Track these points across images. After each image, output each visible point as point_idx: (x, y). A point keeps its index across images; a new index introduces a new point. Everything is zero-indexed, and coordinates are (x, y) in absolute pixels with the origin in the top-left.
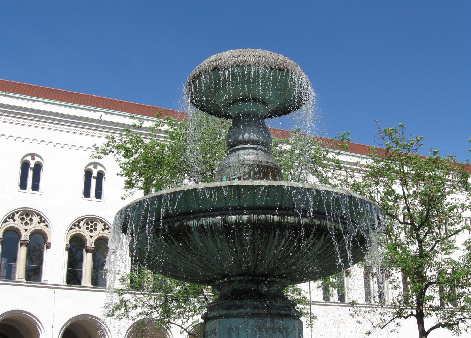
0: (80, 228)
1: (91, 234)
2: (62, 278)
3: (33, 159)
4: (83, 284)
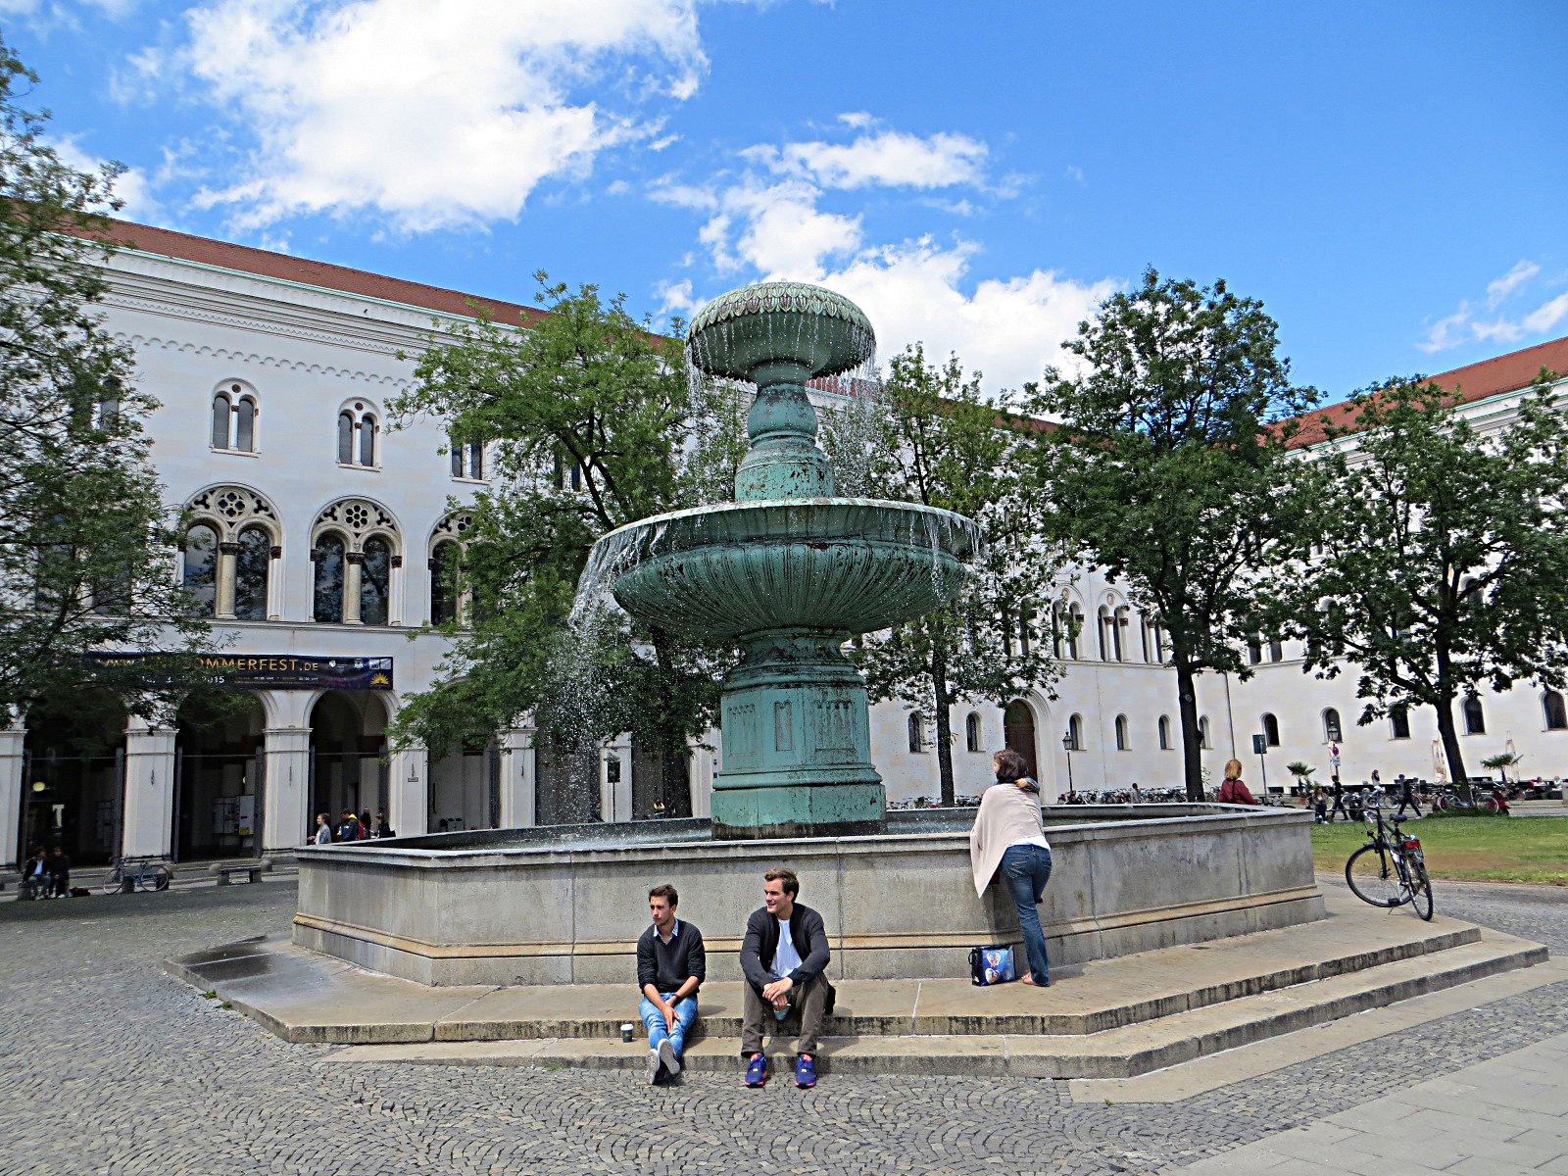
0: (335, 519)
1: (357, 531)
2: (306, 612)
3: (236, 389)
4: (273, 609)
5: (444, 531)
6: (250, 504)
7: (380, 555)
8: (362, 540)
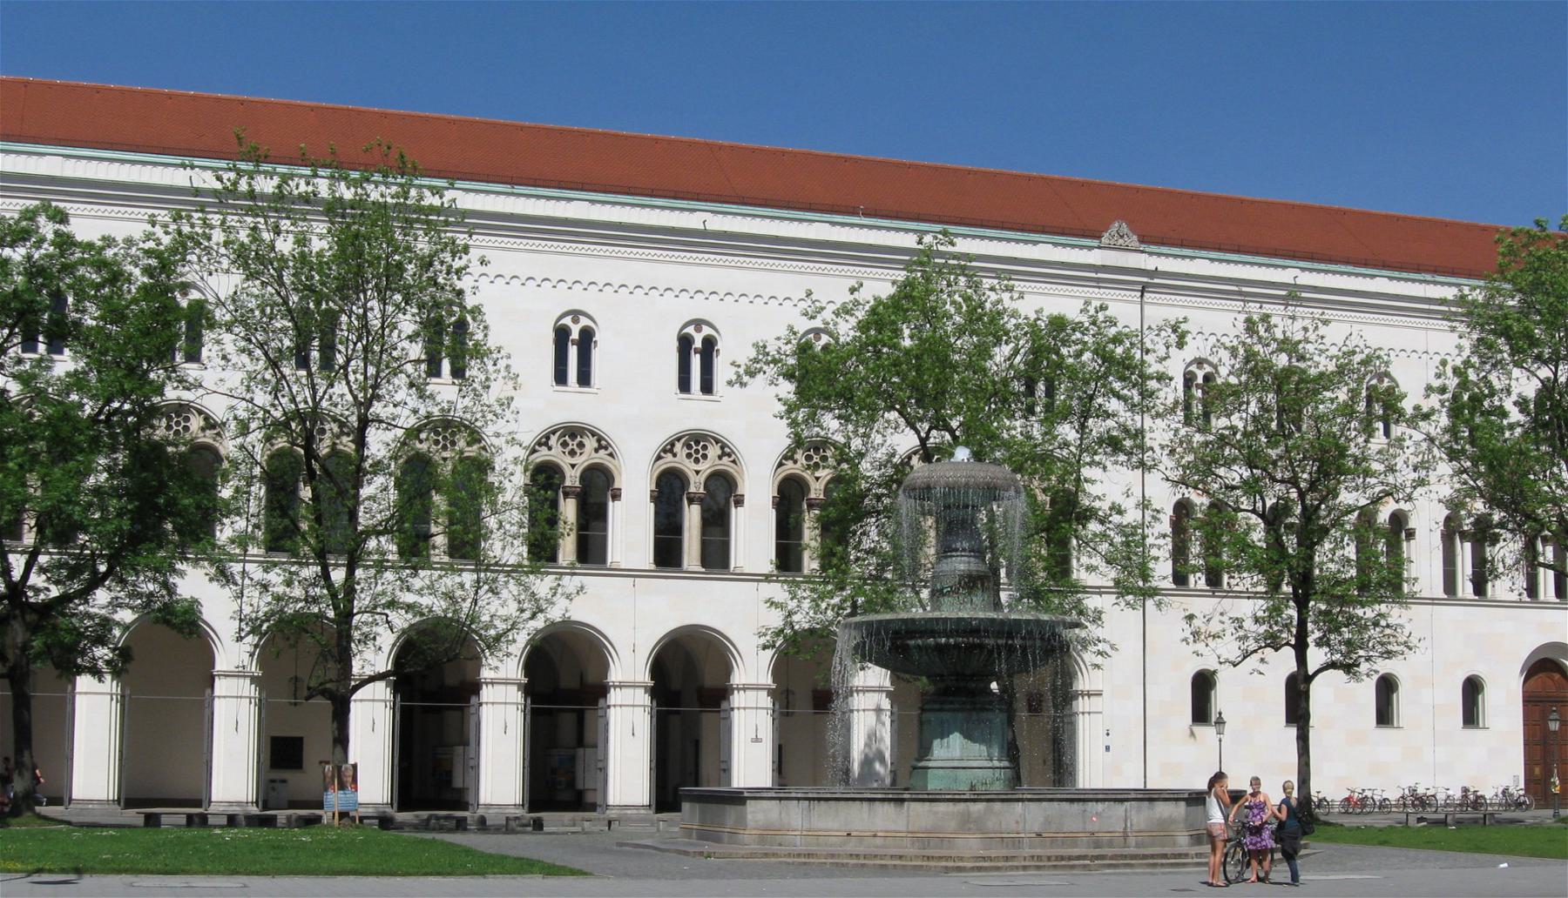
3: (576, 321)
5: (790, 464)
6: (590, 443)
7: (597, 490)
8: (702, 478)
